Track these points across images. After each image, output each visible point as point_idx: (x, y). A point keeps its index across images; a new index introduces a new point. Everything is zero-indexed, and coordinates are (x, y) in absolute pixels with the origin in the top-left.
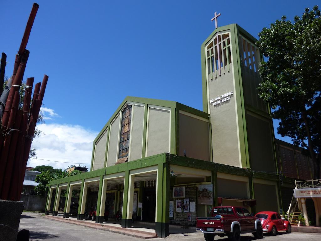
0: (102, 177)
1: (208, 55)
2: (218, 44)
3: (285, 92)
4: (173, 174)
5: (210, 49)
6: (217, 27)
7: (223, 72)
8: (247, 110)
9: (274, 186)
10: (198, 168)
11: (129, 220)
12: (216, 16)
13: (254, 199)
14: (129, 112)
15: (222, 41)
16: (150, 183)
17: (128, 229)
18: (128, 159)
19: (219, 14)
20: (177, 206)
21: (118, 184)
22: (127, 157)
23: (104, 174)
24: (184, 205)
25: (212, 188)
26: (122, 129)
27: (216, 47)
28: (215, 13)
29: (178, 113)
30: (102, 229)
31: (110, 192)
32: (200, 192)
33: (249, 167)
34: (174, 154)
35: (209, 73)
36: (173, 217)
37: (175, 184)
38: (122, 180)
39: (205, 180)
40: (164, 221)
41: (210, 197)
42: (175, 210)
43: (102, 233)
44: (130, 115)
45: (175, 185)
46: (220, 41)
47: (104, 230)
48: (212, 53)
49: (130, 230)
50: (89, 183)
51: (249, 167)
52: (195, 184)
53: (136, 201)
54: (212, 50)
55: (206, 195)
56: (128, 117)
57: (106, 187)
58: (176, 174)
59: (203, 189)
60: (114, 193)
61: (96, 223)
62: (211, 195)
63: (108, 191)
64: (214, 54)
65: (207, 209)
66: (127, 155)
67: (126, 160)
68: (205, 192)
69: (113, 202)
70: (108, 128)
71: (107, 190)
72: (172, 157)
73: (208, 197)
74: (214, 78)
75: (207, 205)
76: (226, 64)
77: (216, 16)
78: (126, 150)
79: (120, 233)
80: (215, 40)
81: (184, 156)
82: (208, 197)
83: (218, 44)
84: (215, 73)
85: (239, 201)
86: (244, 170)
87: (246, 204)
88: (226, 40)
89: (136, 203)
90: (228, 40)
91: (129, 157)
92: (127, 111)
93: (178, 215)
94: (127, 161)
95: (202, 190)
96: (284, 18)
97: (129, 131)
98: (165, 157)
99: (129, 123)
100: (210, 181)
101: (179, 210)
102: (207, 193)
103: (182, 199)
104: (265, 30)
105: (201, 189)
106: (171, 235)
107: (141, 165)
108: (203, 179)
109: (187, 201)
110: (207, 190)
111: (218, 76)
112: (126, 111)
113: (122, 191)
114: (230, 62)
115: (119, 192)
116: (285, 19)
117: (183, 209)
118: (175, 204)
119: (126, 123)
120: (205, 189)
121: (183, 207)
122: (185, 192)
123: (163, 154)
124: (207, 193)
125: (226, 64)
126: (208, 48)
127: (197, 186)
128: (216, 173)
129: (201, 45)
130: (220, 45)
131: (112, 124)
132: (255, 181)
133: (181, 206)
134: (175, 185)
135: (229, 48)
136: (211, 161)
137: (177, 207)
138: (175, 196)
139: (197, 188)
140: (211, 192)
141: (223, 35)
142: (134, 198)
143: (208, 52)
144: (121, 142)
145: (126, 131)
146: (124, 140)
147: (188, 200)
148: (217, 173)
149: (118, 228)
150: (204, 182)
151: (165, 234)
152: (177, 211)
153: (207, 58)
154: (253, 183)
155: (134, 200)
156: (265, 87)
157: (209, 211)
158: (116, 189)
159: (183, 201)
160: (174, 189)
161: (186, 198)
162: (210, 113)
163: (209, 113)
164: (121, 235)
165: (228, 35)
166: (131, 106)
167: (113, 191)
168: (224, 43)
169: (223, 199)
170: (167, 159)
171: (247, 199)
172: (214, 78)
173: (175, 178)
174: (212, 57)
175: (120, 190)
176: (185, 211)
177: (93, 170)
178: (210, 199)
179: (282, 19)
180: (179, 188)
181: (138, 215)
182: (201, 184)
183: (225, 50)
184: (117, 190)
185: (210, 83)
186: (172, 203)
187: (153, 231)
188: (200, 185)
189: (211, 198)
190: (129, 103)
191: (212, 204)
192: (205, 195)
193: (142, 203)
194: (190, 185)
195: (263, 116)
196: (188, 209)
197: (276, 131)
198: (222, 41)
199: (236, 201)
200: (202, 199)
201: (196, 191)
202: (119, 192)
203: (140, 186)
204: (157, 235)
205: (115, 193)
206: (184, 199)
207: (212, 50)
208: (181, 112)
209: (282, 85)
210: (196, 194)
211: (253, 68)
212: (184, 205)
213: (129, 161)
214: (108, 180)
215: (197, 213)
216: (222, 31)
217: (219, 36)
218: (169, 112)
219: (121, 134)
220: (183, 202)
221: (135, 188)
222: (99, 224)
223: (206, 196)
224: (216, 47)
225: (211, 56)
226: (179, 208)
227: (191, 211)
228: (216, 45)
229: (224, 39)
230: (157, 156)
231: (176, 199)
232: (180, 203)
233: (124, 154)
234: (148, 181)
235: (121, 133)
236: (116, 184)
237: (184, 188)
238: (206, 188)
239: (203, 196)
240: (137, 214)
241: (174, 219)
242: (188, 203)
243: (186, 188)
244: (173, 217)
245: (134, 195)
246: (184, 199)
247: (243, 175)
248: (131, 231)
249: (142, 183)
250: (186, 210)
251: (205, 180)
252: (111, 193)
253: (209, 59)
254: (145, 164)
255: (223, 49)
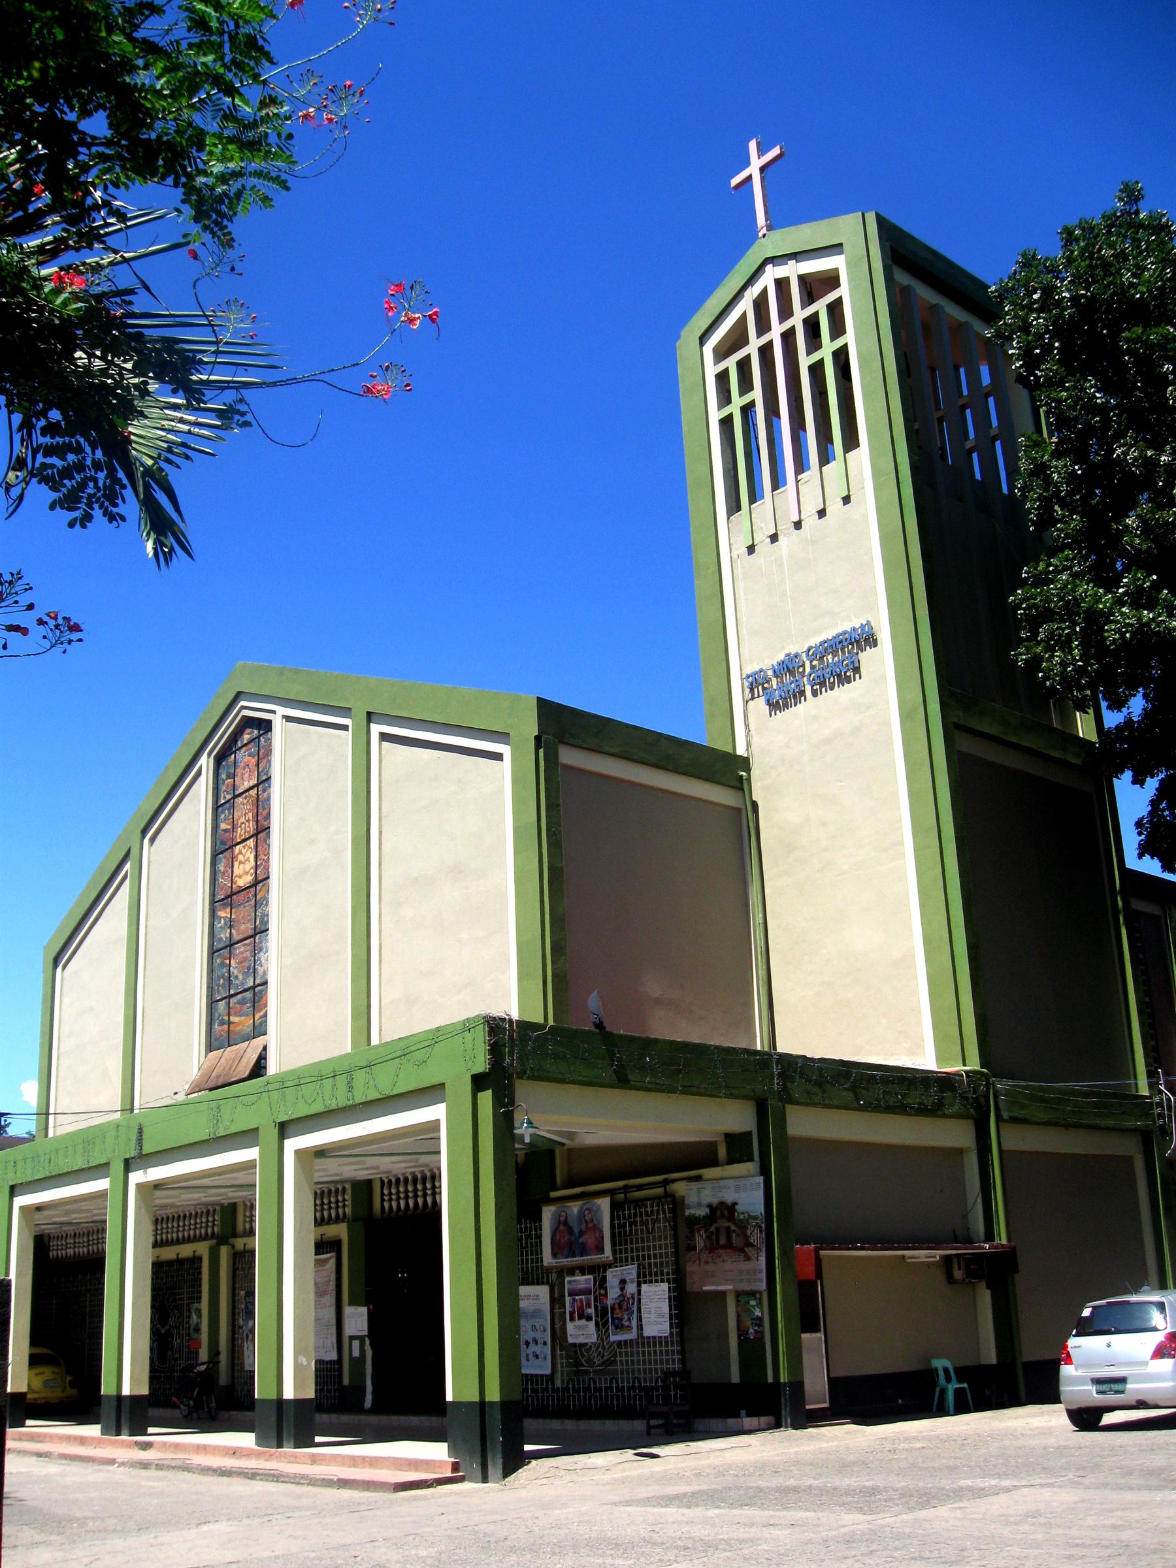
0: (118, 1167)
1: (725, 398)
2: (777, 330)
3: (1143, 627)
4: (532, 1130)
5: (731, 363)
6: (770, 228)
7: (811, 505)
8: (957, 726)
9: (1129, 1160)
10: (671, 1090)
11: (297, 1403)
12: (756, 164)
13: (1004, 1241)
14: (254, 761)
15: (800, 314)
16: (406, 1191)
17: (295, 1456)
18: (265, 1048)
19: (776, 151)
20: (568, 1309)
21: (214, 1204)
22: (258, 1042)
23: (132, 1153)
24: (609, 1302)
25: (759, 1195)
26: (221, 867)
27: (766, 351)
28: (753, 146)
29: (552, 761)
30: (145, 1465)
31: (169, 1253)
32: (693, 1221)
33: (974, 1065)
34: (542, 1021)
35: (734, 506)
36: (548, 1372)
37: (556, 1189)
38: (241, 1178)
39: (722, 1152)
40: (493, 1394)
41: (752, 1245)
42: (558, 1336)
43: (151, 1480)
44: (264, 782)
45: (553, 1194)
46: (786, 312)
47: (159, 1467)
48: (746, 385)
49: (305, 1454)
50: (39, 1208)
51: (974, 1065)
52: (666, 1182)
53: (330, 1299)
54: (744, 366)
55: (729, 1238)
56: (253, 792)
57: (149, 1227)
58: (559, 1133)
59: (710, 1206)
60: (196, 1260)
61: (102, 1434)
62: (757, 1237)
63: (159, 1251)
64: (757, 394)
65: (738, 1316)
66: (259, 1030)
67: (255, 1057)
68: (723, 1223)
69: (194, 1317)
70: (128, 867)
71: (156, 1245)
72: (524, 1039)
73: (743, 1249)
74: (761, 537)
75: (739, 1294)
76: (825, 458)
77: (756, 164)
78: (248, 995)
79: (253, 1475)
80: (760, 304)
81: (589, 1027)
82: (742, 1250)
83: (777, 330)
84: (764, 507)
85: (922, 1255)
86: (945, 1082)
87: (958, 1274)
88: (820, 307)
89: (331, 1313)
90: (835, 309)
91: (272, 1038)
92: (243, 757)
93: (578, 1363)
94: (259, 1069)
95: (702, 1212)
96: (1132, 195)
97: (260, 880)
98: (479, 1044)
99: (261, 831)
100: (751, 1159)
101: (582, 1332)
102: (733, 1228)
103: (598, 1271)
104: (1028, 262)
105: (699, 1204)
106: (534, 1462)
107: (351, 1089)
108: (713, 1145)
109: (623, 1282)
110: (732, 1208)
111: (785, 527)
112: (240, 754)
113: (239, 1243)
114: (851, 441)
115: (224, 1251)
116: (1136, 201)
117: (601, 1326)
118: (556, 1301)
119: (240, 833)
120: (722, 1203)
121: (602, 1312)
122: (612, 1226)
123: (467, 1026)
124: (733, 1228)
125: (825, 458)
126: (722, 353)
127: (680, 1188)
128: (784, 1107)
129: (678, 337)
130: (788, 337)
131: (152, 840)
132: (1021, 1140)
133: (591, 1311)
134: (553, 1194)
135: (841, 357)
136: (759, 1048)
137: (572, 1319)
138: (555, 1255)
139: (677, 1203)
140: (755, 1218)
141: (802, 279)
142: (316, 1284)
143: (722, 377)
144: (219, 951)
145: (242, 882)
146: (236, 937)
147: (631, 1271)
148: (787, 1105)
149: (234, 1452)
150: (714, 1163)
151: (500, 1461)
152: (570, 1340)
153: (715, 416)
154: (1000, 1151)
155: (320, 1293)
156: (1035, 606)
157: (749, 1323)
158: (205, 1238)
159: (604, 1280)
160: (548, 1213)
161: (617, 1262)
162: (749, 745)
163: (741, 751)
164: (258, 1486)
165: (831, 280)
166: (265, 726)
167: (186, 1251)
168: (812, 325)
169: (822, 1252)
170: (495, 1050)
171: (969, 1241)
172: (761, 537)
173: (551, 1153)
174: (747, 410)
175: (232, 1240)
176: (613, 1338)
177: (51, 1134)
178: (748, 1258)
179: (1121, 200)
180: (575, 1207)
181: (346, 1382)
182: (698, 1178)
183: (817, 370)
184: (214, 1242)
185: (739, 573)
186: (535, 1297)
187: (438, 1451)
188: (695, 1185)
189: (759, 1250)
190: (251, 708)
191: (763, 1286)
192: (723, 1241)
193: (364, 1310)
194: (640, 1187)
195: (1056, 754)
196: (634, 1323)
197: (1131, 840)
198: (800, 314)
199: (903, 1257)
200: (707, 1263)
201: (675, 1218)
202: (224, 1251)
203: (348, 1210)
204: (455, 1467)
205: (200, 1259)
206: (605, 1266)
207: (744, 366)
208: (569, 756)
209: (1125, 594)
210: (676, 1237)
211: (989, 464)
212: (609, 1302)
213: (272, 1068)
214: (158, 1185)
215: (682, 1343)
216: (796, 256)
217: (782, 285)
218: (498, 757)
219: (213, 902)
220: (602, 1283)
221: (319, 1222)
222: (123, 1441)
223: (729, 1246)
224: (766, 351)
225: (738, 402)
226: (583, 1322)
227: (649, 1331)
228: (764, 340)
229: (809, 297)
230: (437, 1036)
231: (563, 1272)
232: (587, 1292)
233: (241, 1022)
234: (398, 1180)
235: (213, 894)
236: (207, 1204)
237: (604, 1204)
238: (729, 1197)
239: (713, 1247)
240: (340, 1376)
241: (558, 1384)
242: (631, 1288)
243: (615, 1206)
244: (548, 1372)
245: (318, 1263)
246: (605, 1266)
247: (933, 1111)
248: (314, 1460)
249: (363, 1188)
250: (619, 1327)
251: (722, 1152)
252: (180, 1262)
253: (726, 423)
254: (386, 1082)
255: (805, 362)
